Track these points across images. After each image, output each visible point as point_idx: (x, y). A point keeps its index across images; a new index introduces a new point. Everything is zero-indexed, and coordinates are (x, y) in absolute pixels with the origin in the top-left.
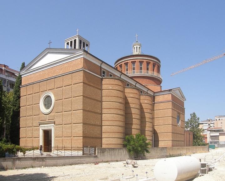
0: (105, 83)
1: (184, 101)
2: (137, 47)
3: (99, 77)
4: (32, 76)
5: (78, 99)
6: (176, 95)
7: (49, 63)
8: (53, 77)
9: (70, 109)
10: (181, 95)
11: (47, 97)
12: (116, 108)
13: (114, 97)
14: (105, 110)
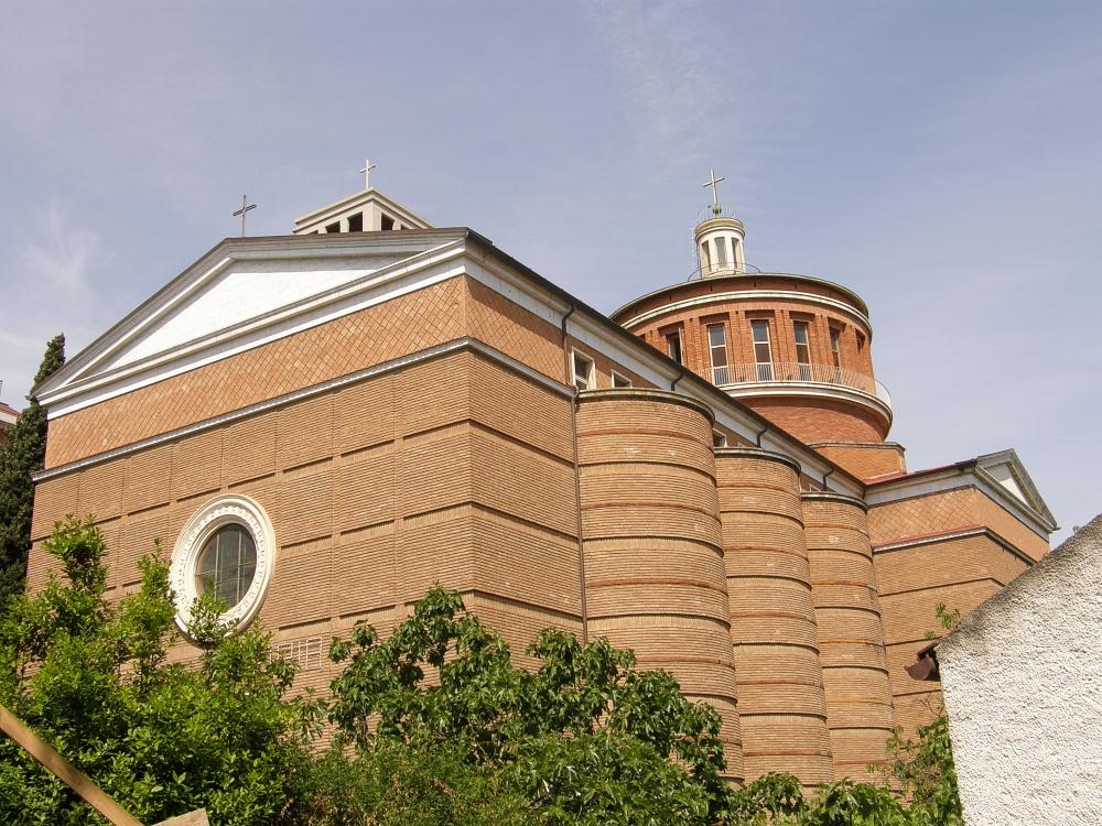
0: (595, 425)
1: (1048, 532)
2: (720, 241)
4: (121, 407)
5: (439, 526)
7: (243, 324)
8: (266, 401)
11: (220, 530)
12: (679, 576)
13: (659, 511)
14: (606, 592)
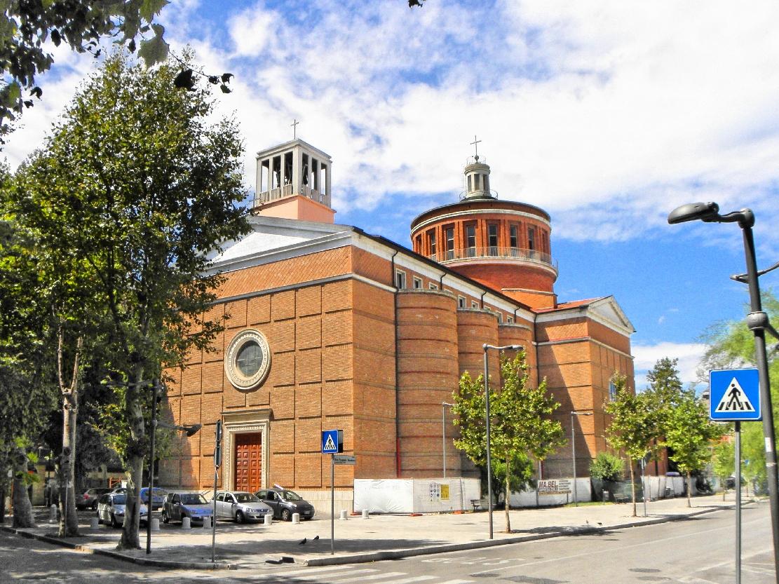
3: (388, 291)
6: (602, 319)
9: (317, 377)
10: (619, 316)
